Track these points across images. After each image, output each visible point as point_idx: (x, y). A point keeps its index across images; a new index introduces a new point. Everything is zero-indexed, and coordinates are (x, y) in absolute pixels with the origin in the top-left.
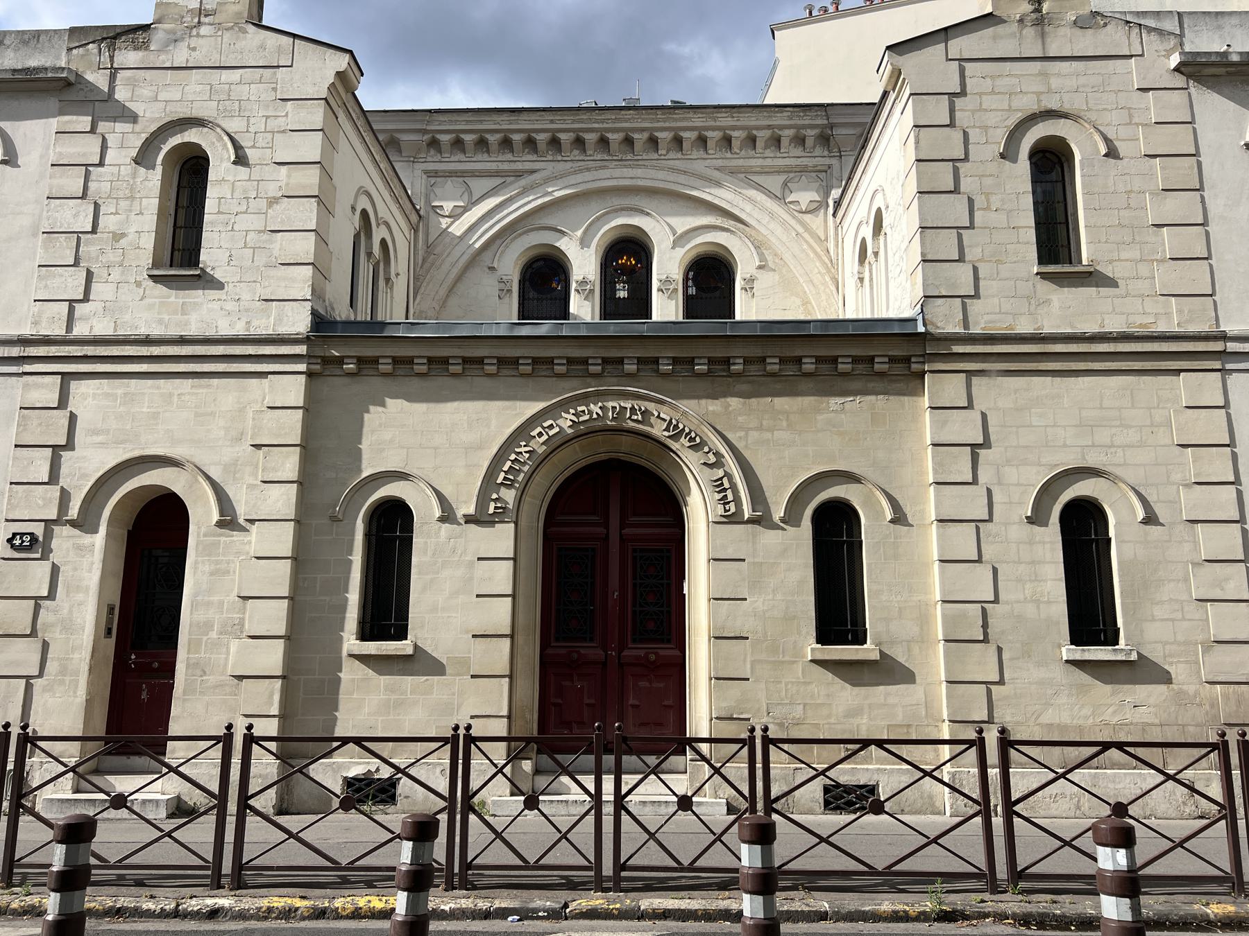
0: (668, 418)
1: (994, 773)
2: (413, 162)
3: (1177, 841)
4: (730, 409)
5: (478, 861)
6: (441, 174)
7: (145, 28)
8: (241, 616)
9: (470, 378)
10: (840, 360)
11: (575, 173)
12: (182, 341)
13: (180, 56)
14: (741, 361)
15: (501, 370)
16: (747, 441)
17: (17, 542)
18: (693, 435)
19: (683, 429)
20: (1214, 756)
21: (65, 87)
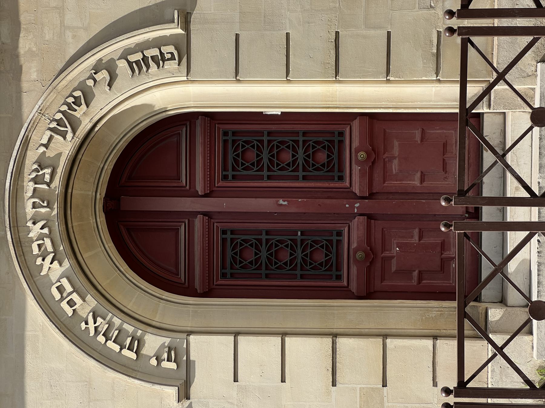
0: (49, 133)
18: (71, 100)
19: (63, 113)
20: (476, 39)
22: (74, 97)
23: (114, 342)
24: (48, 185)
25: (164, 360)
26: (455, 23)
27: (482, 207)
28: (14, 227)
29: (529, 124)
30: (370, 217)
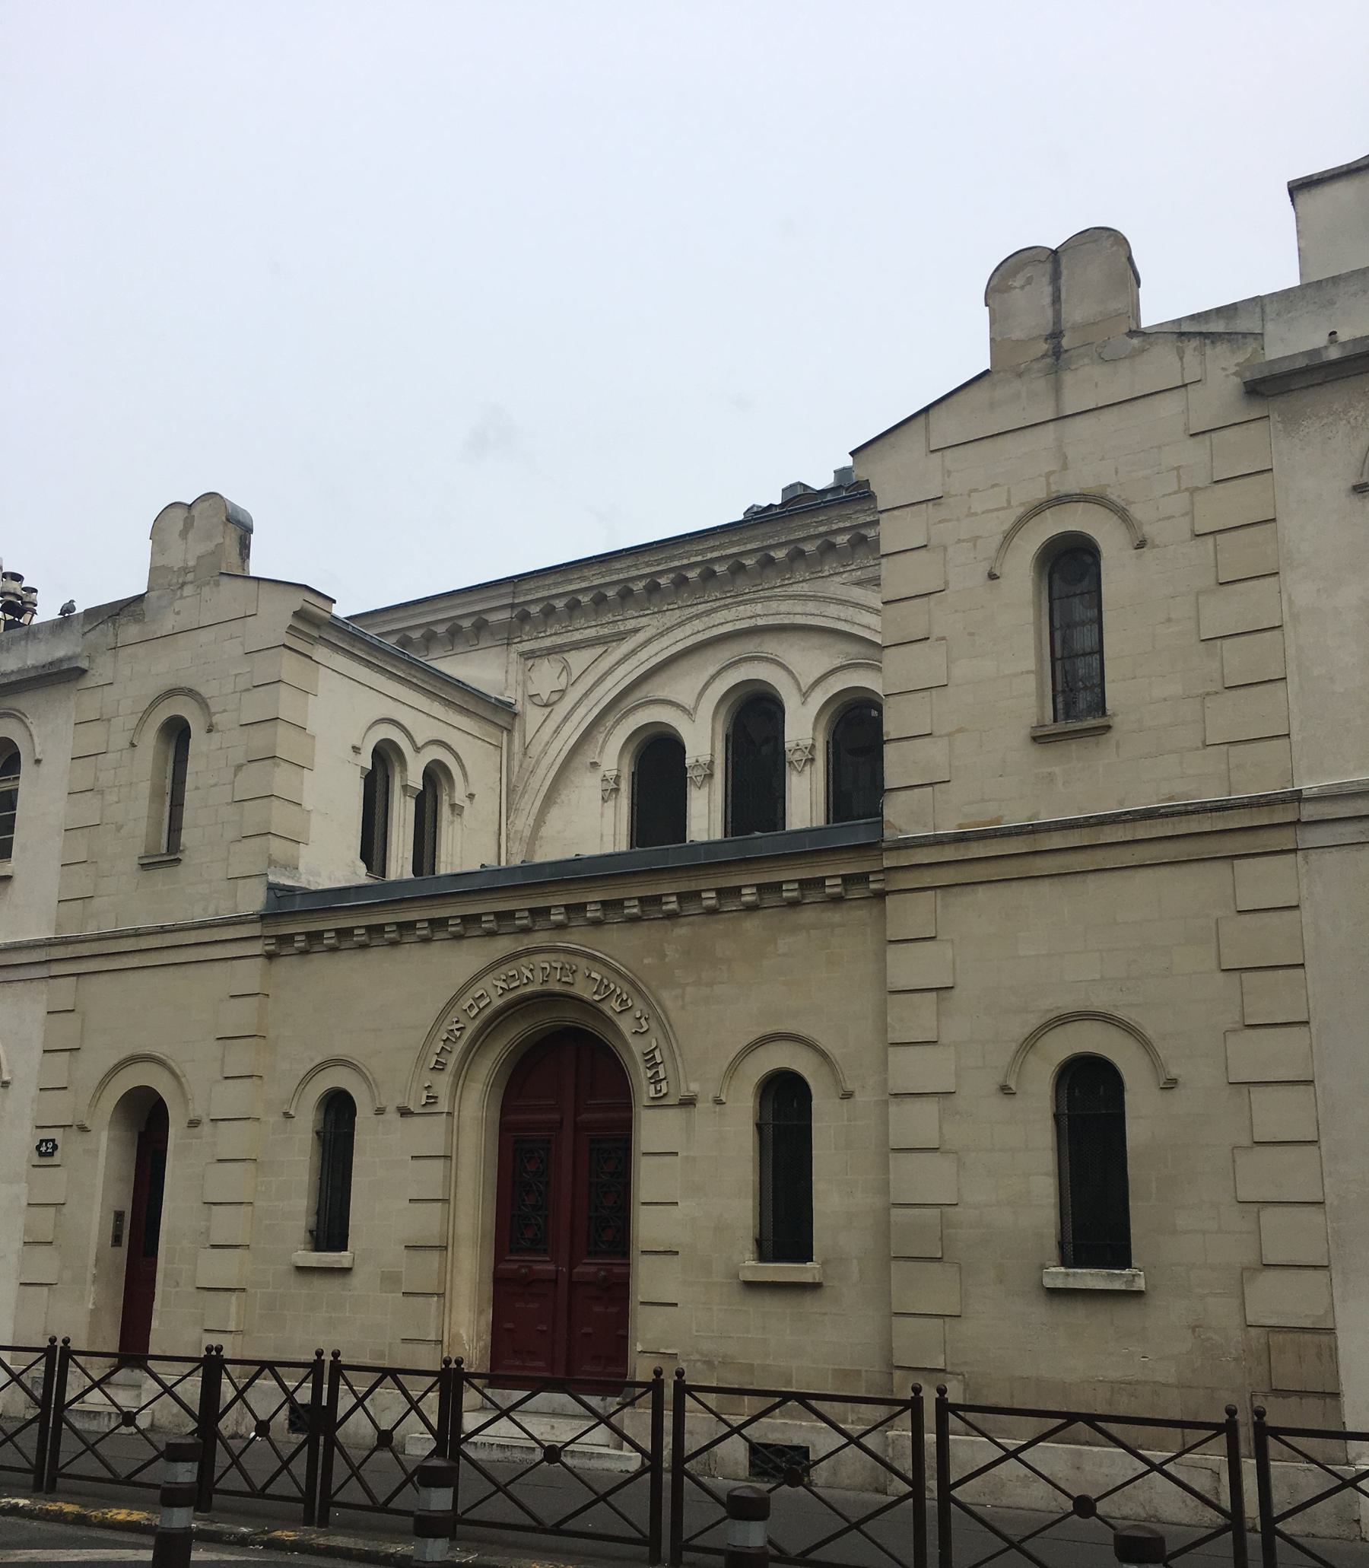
0: (599, 978)
1: (930, 1438)
2: (508, 644)
3: (854, 1520)
4: (667, 960)
5: (470, 1516)
6: (538, 653)
7: (140, 598)
8: (208, 1224)
9: (407, 945)
10: (784, 887)
11: (680, 624)
12: (163, 930)
13: (169, 624)
14: (674, 899)
15: (436, 934)
16: (683, 1000)
17: (43, 1149)
18: (625, 997)
19: (615, 990)
20: (1223, 1437)
21: (80, 675)
22: (627, 1000)
23: (443, 1047)
24: (559, 980)
25: (428, 1093)
26: (1244, 1418)
27: (120, 1351)
28: (528, 952)
29: (1075, 1496)
30: (556, 1281)
